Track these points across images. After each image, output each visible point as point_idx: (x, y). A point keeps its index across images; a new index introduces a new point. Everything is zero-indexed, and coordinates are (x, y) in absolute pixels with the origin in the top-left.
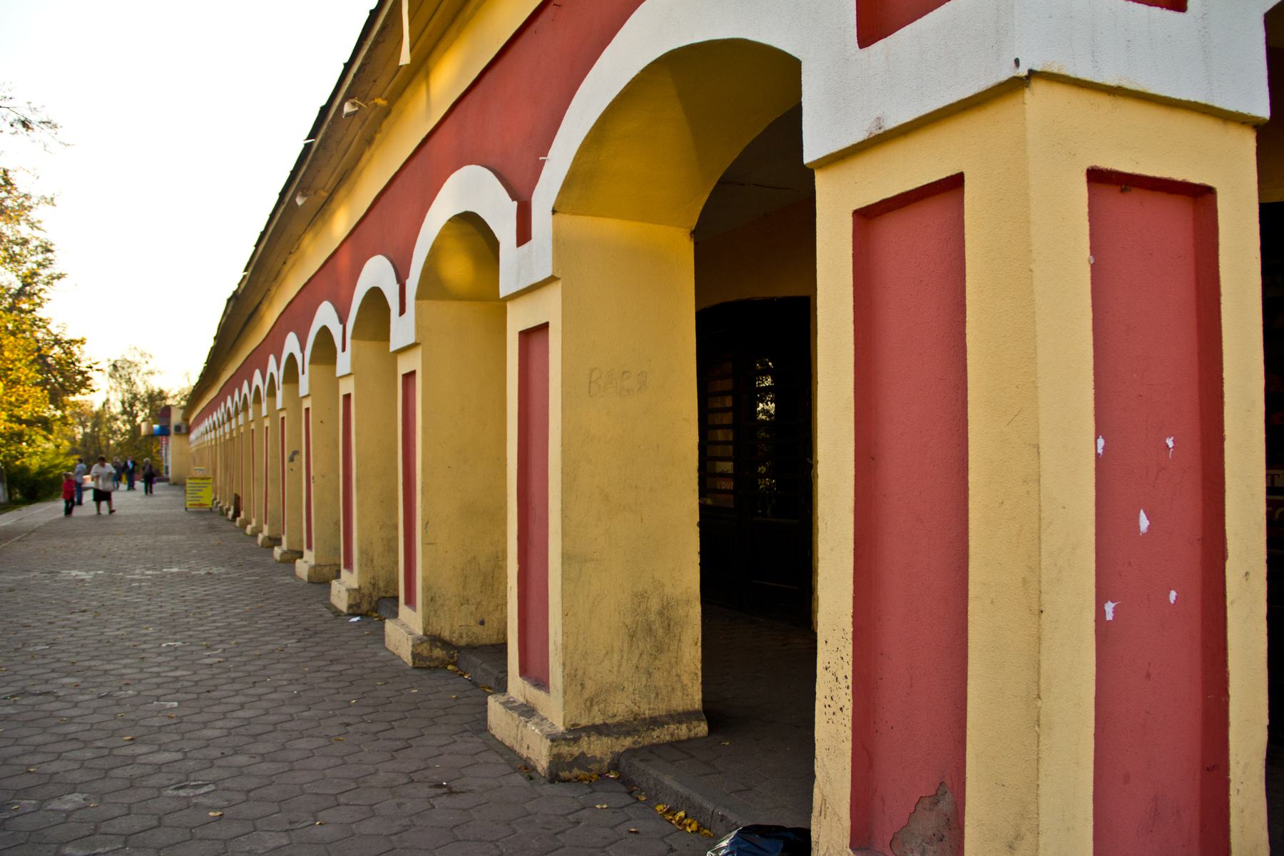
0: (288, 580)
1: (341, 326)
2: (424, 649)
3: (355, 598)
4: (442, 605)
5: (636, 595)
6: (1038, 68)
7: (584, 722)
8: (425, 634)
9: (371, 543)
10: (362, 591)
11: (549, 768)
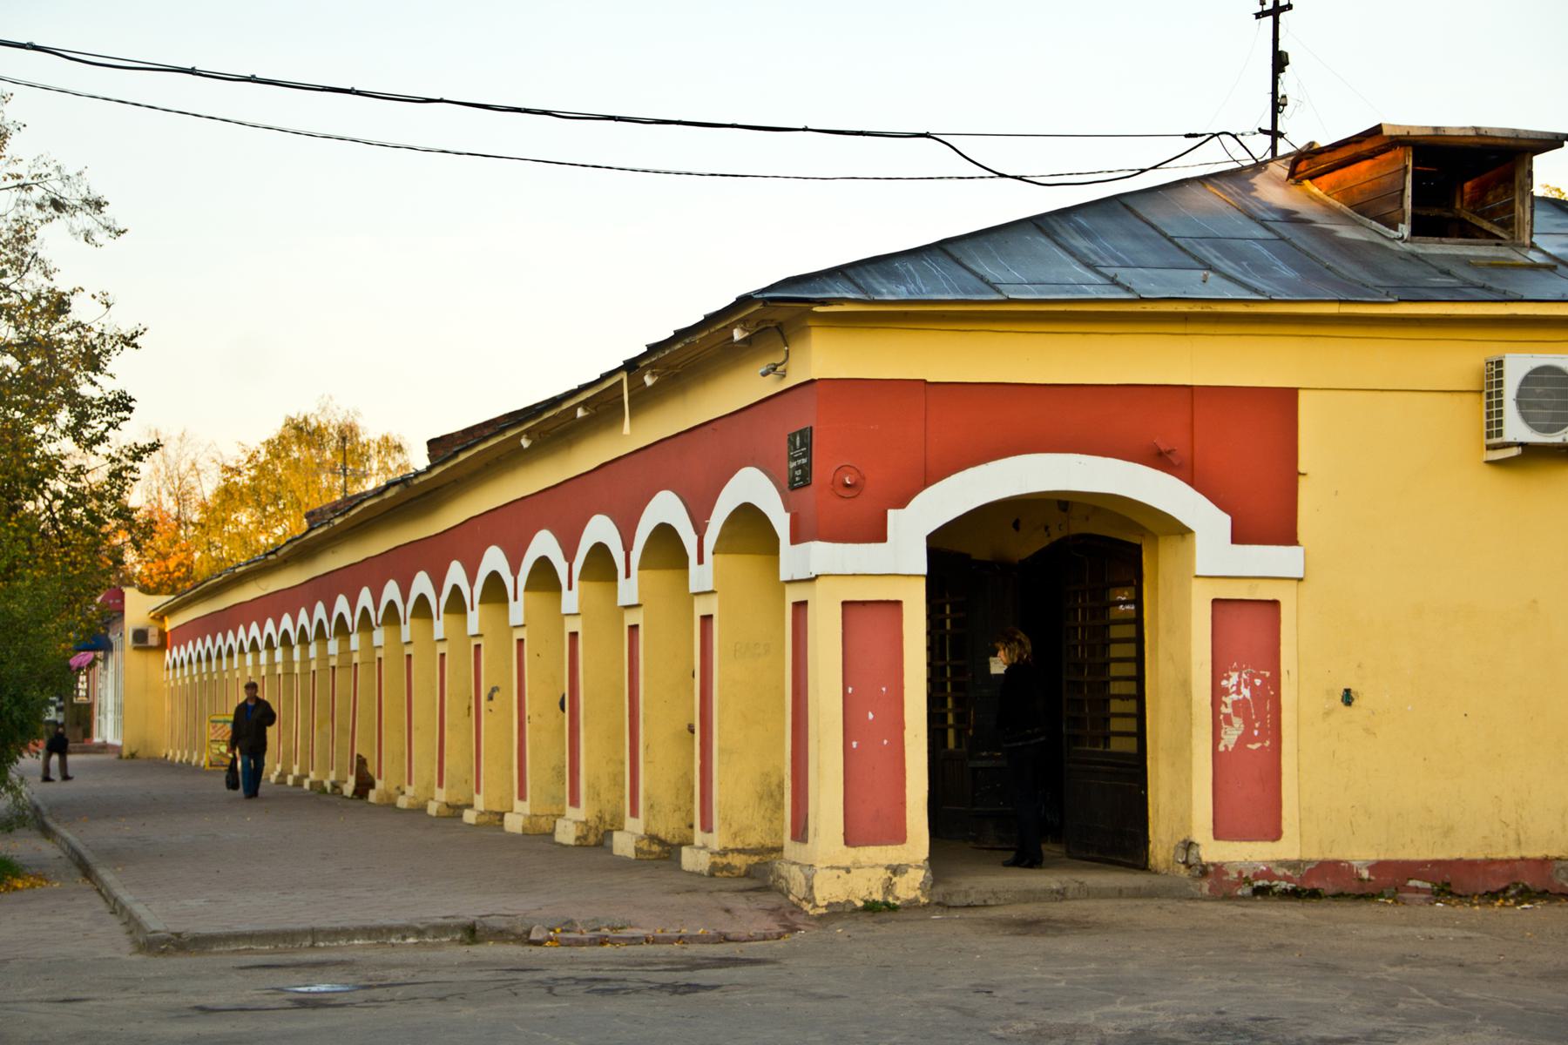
0: (502, 834)
1: (567, 564)
2: (645, 845)
3: (582, 830)
4: (659, 812)
5: (763, 774)
6: (819, 573)
7: (731, 846)
8: (646, 834)
9: (598, 778)
10: (589, 824)
11: (709, 870)
